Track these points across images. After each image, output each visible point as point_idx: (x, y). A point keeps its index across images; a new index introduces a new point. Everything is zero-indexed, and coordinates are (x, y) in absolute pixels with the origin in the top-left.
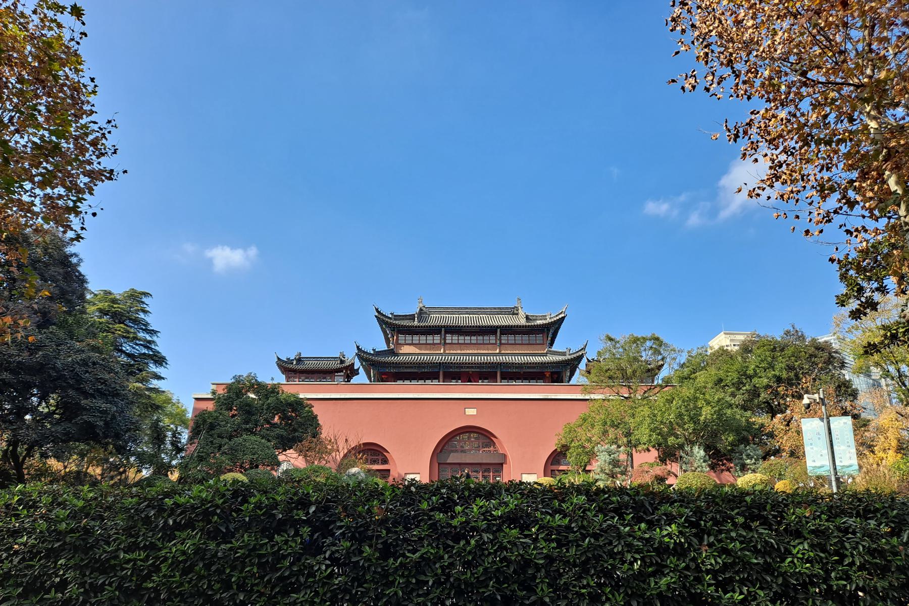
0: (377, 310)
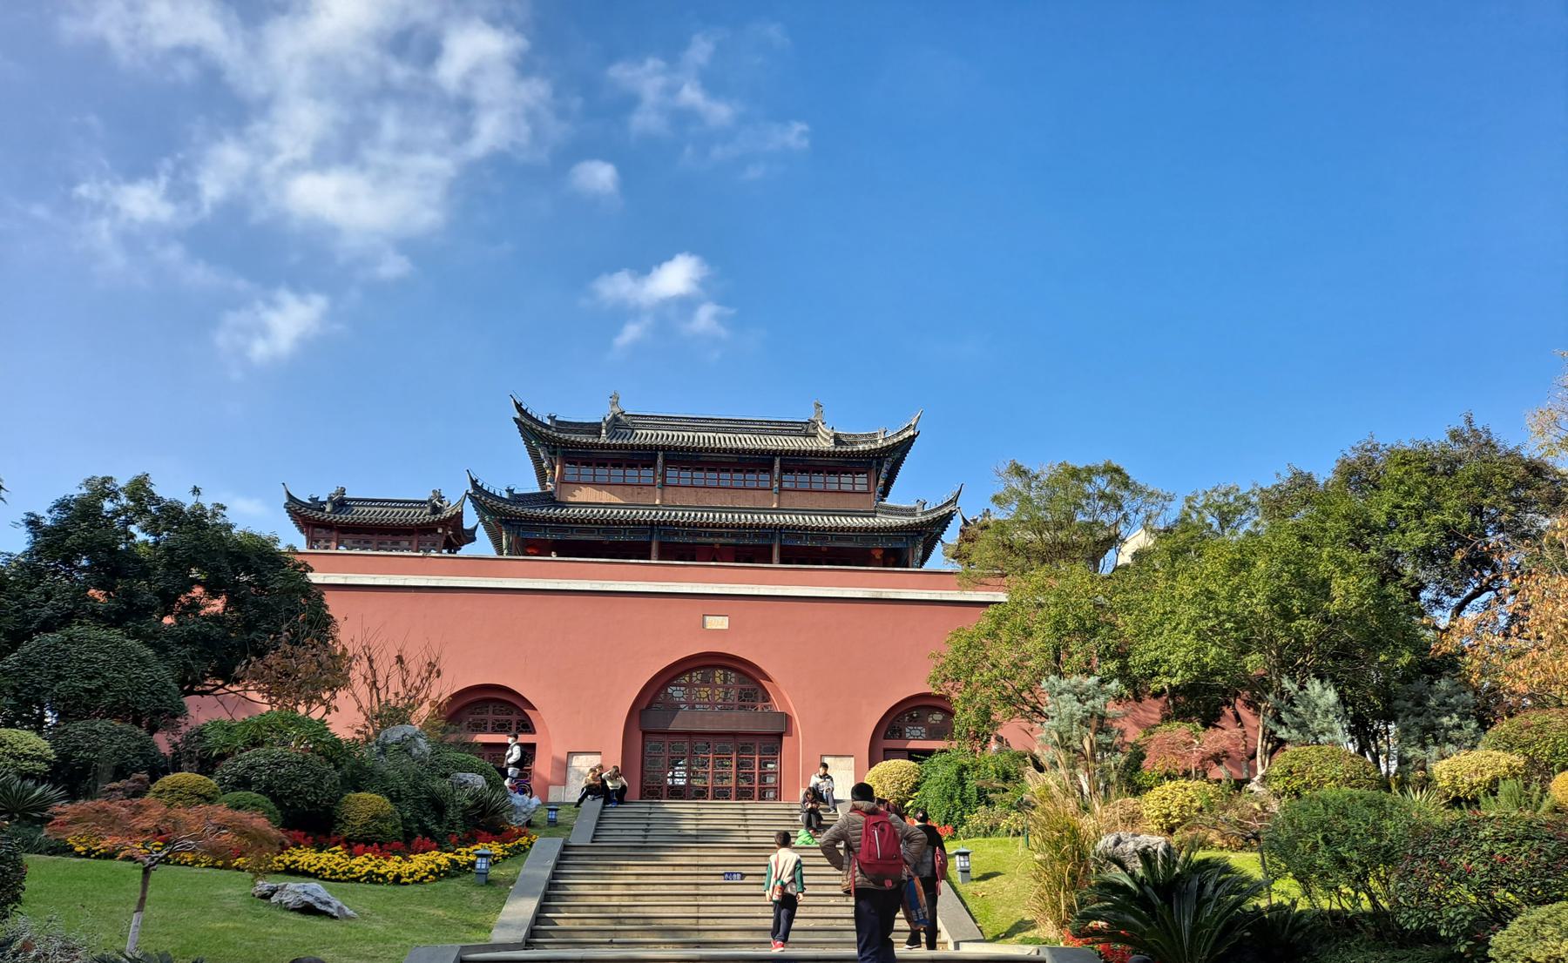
0: (519, 407)
